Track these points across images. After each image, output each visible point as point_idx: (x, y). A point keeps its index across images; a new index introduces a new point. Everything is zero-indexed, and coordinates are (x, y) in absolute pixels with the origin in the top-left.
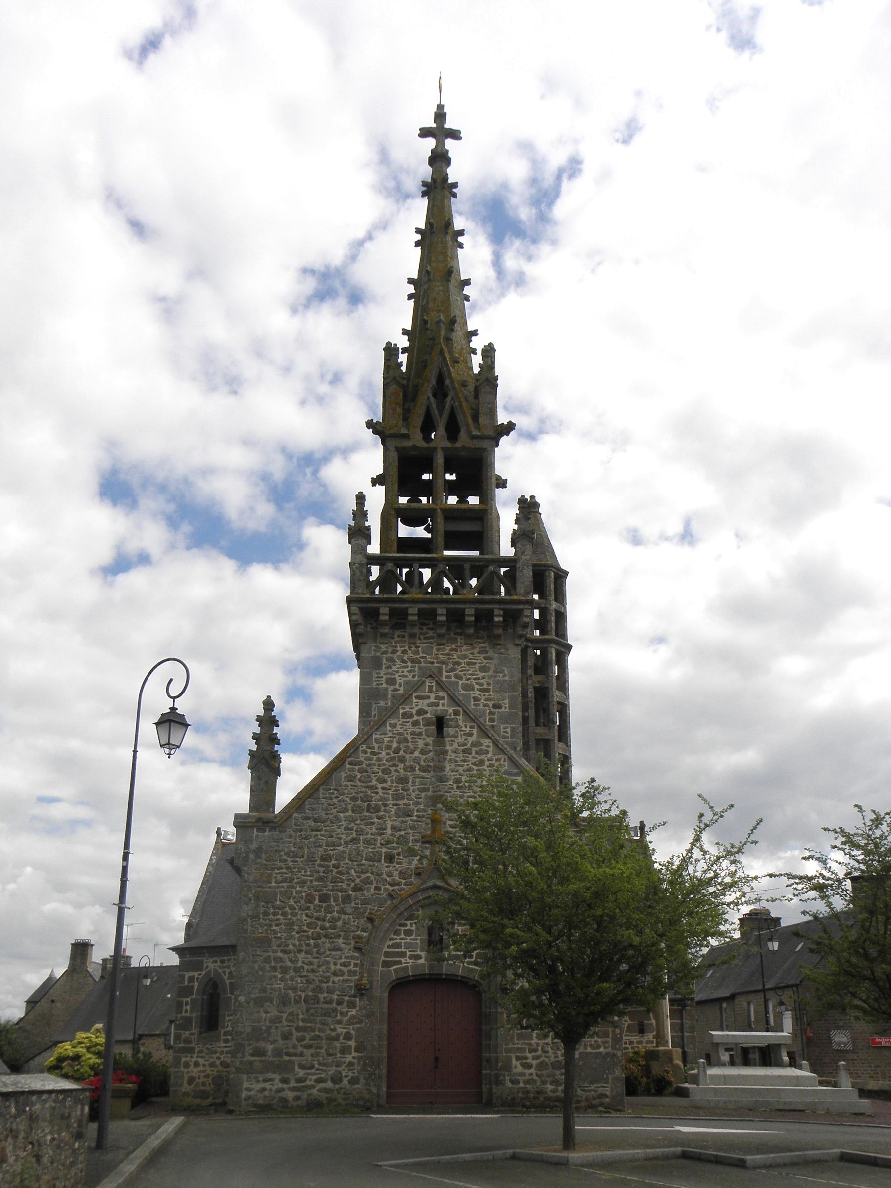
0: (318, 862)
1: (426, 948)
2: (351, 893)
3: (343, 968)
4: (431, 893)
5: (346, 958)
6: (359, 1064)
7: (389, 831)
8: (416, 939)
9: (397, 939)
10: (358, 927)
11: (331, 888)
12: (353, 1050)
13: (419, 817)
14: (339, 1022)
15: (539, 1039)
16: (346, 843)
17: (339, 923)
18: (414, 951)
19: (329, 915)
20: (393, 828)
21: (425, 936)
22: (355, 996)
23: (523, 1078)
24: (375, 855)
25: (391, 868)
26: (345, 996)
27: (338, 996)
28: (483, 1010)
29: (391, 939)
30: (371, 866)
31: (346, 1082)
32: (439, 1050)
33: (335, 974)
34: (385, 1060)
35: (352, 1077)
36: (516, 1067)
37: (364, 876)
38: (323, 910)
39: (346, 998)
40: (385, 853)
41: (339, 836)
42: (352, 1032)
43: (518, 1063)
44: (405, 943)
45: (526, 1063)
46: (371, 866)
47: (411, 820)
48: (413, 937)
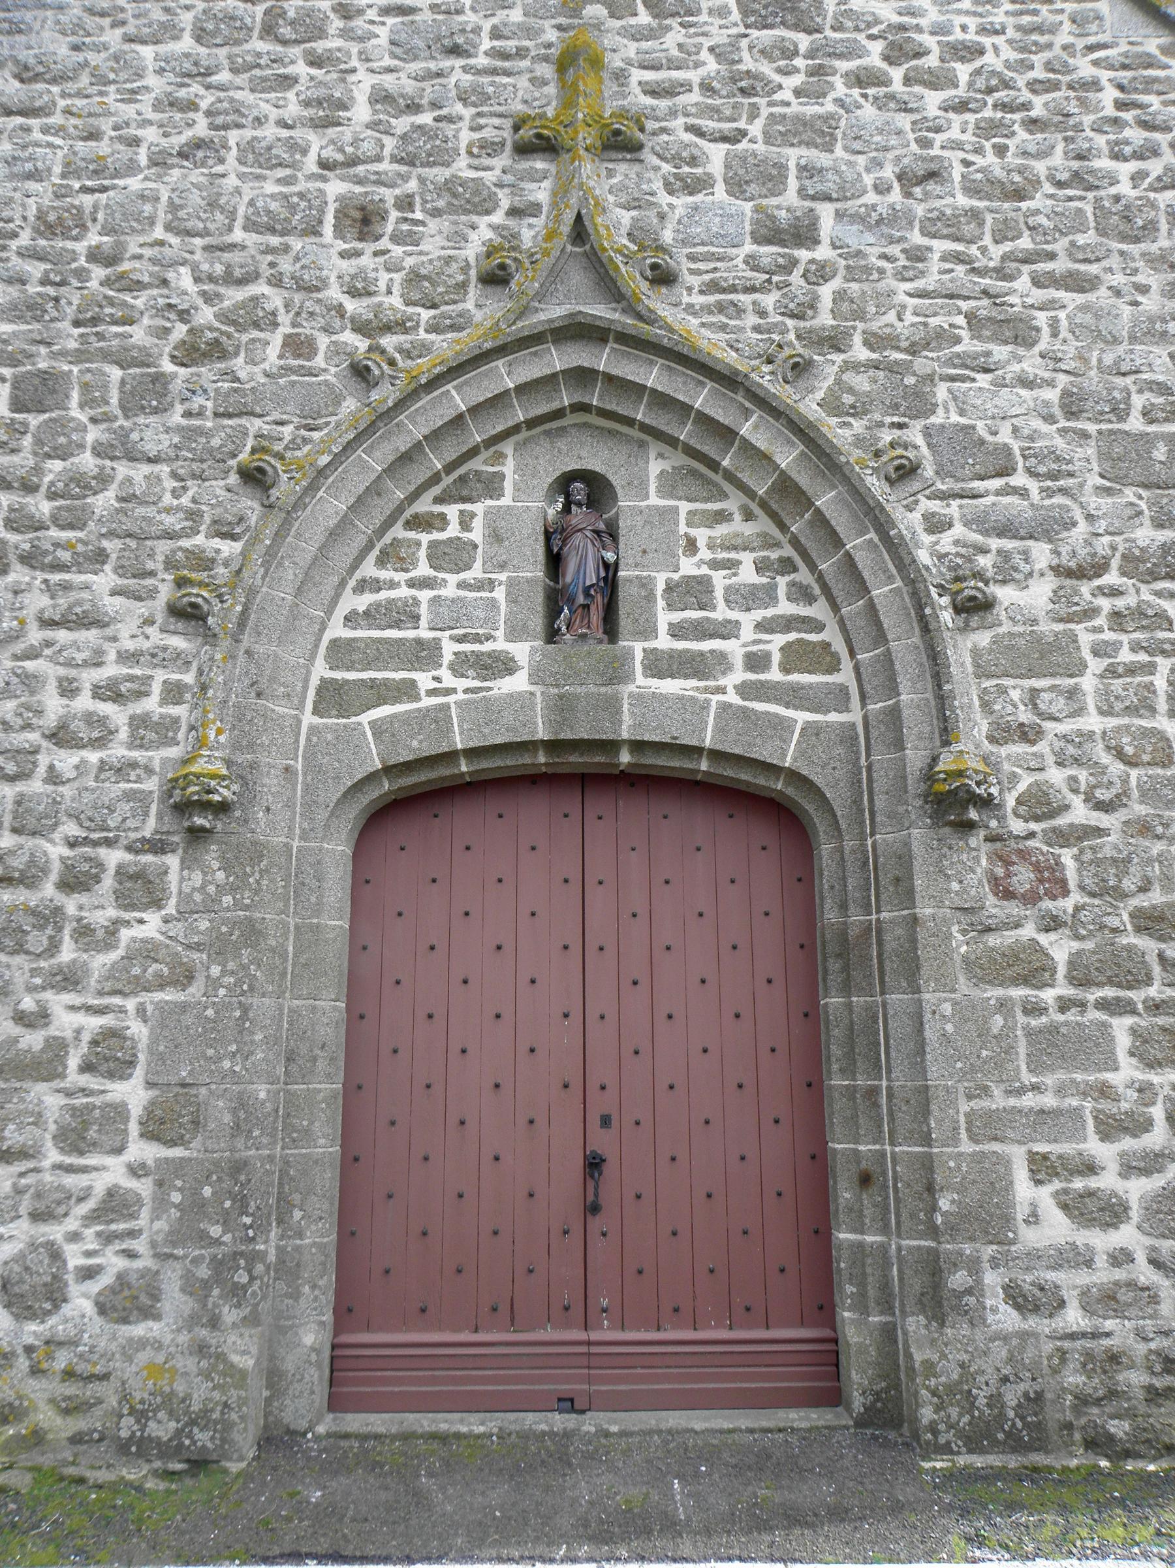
0: (25, 239)
1: (537, 622)
2: (168, 367)
3: (107, 708)
4: (557, 359)
5: (126, 657)
6: (161, 1205)
7: (361, 112)
8: (491, 585)
9: (393, 585)
10: (193, 515)
11: (72, 345)
12: (134, 1128)
13: (505, 56)
14: (68, 979)
15: (1152, 1064)
16: (159, 161)
17: (104, 502)
18: (477, 639)
19: (56, 465)
20: (381, 98)
21: (534, 571)
22: (158, 846)
23: (1083, 1278)
24: (293, 208)
25: (366, 261)
26: (109, 843)
27: (72, 844)
28: (830, 915)
29: (363, 586)
30: (269, 250)
31: (88, 1306)
32: (606, 1121)
33: (61, 736)
34: (327, 1180)
35: (121, 1277)
36: (1034, 1218)
37: (235, 296)
38: (27, 441)
39: (114, 857)
40: (340, 199)
41: (132, 131)
42: (138, 1030)
43: (1045, 1195)
44: (435, 600)
45: (1091, 1194)
46: (269, 250)
47: (465, 69)
48: (476, 572)
